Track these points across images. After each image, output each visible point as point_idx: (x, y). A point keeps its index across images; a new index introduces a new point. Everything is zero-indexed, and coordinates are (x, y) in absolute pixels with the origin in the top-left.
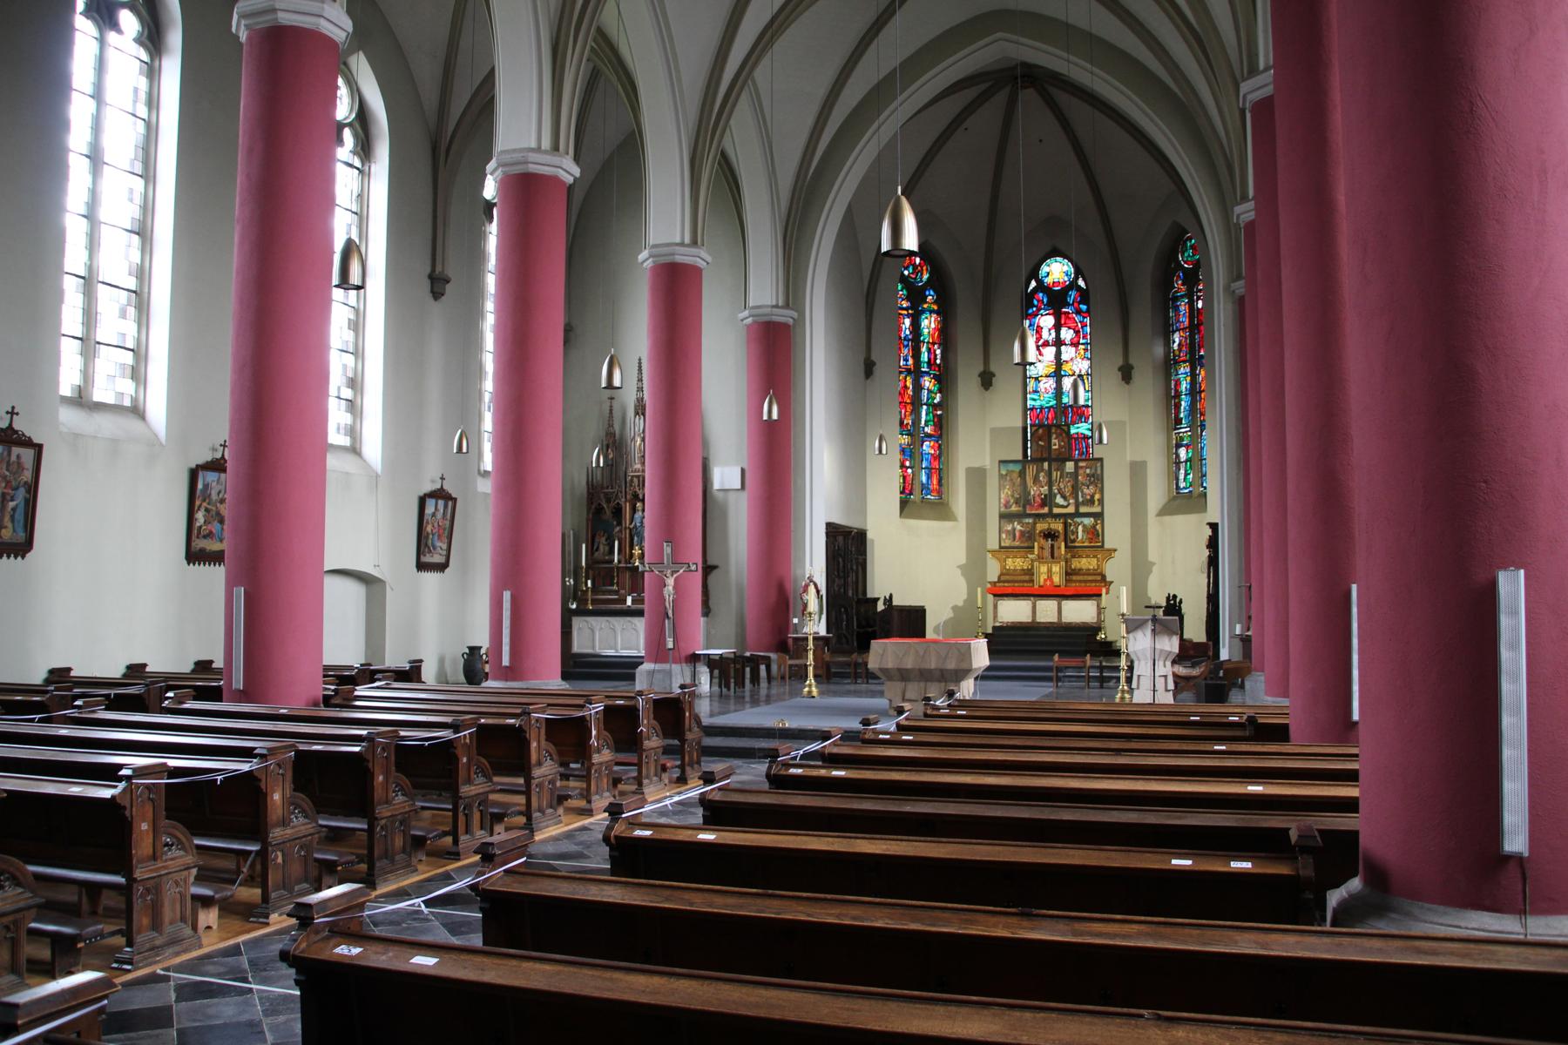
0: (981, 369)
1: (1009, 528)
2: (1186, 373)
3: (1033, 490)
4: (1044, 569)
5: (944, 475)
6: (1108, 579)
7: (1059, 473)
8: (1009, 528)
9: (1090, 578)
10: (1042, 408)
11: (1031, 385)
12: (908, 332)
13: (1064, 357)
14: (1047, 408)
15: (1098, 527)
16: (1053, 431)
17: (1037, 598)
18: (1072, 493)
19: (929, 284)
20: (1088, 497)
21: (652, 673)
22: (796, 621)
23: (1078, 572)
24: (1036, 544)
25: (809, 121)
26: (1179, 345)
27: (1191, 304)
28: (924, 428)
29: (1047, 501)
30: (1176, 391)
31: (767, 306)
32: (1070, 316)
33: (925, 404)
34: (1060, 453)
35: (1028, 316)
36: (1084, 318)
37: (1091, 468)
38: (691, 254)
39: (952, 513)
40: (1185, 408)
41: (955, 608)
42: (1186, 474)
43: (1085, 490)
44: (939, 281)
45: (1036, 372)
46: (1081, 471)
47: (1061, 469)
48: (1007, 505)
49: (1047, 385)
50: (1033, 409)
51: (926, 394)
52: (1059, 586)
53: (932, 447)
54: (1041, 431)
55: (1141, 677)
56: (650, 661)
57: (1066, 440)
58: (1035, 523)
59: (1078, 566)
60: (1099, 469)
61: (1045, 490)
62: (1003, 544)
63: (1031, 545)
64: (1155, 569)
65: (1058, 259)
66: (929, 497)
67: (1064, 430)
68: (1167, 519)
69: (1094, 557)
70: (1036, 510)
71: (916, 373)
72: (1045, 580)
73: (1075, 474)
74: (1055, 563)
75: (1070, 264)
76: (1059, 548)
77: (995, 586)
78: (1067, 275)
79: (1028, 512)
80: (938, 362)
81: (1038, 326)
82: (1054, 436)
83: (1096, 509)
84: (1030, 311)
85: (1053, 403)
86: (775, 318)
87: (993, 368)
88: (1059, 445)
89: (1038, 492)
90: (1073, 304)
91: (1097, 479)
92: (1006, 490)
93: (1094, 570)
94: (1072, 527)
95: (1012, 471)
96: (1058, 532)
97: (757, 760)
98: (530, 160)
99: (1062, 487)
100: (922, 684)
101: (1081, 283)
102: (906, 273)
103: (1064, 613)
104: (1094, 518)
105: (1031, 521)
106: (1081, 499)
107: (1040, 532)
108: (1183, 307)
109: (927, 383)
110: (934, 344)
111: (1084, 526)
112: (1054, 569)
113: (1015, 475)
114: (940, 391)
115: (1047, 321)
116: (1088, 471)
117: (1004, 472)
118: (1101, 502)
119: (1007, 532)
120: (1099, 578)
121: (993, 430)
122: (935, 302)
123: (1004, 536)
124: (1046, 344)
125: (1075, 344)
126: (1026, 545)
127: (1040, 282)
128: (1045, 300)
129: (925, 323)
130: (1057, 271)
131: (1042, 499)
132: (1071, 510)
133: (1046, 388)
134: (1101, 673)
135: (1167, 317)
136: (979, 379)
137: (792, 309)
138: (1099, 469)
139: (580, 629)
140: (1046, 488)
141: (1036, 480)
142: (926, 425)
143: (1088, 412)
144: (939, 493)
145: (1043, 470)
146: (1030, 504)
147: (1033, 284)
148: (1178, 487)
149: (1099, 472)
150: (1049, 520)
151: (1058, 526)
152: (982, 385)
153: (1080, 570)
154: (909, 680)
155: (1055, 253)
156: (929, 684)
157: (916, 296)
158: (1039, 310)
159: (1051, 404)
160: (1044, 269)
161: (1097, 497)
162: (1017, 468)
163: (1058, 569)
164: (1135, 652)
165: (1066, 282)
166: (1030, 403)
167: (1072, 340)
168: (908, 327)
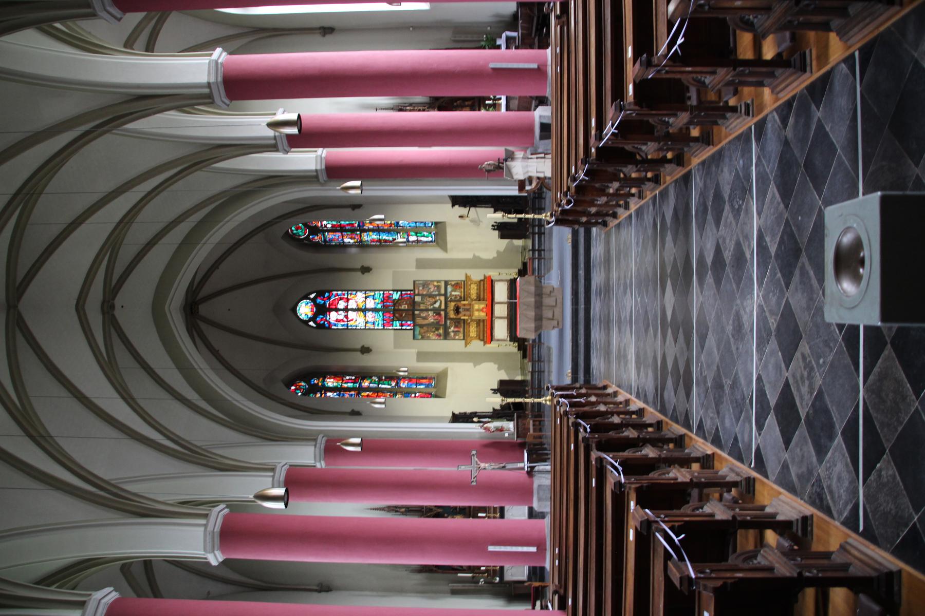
0: (359, 353)
1: (452, 334)
2: (367, 235)
3: (431, 320)
4: (476, 314)
5: (420, 376)
6: (483, 278)
8: (452, 334)
9: (482, 288)
10: (384, 320)
11: (370, 326)
12: (335, 394)
13: (354, 307)
14: (383, 317)
15: (453, 283)
18: (433, 297)
19: (308, 382)
20: (436, 288)
21: (540, 500)
22: (506, 435)
24: (462, 318)
25: (205, 422)
26: (351, 239)
27: (329, 231)
29: (437, 312)
30: (377, 241)
31: (315, 450)
33: (378, 385)
34: (410, 304)
35: (329, 328)
36: (332, 294)
38: (280, 472)
39: (443, 371)
40: (387, 236)
41: (499, 369)
42: (424, 236)
44: (306, 376)
46: (421, 292)
47: (419, 304)
48: (439, 335)
53: (404, 382)
54: (397, 315)
55: (538, 170)
56: (531, 500)
57: (403, 301)
58: (451, 319)
60: (420, 282)
61: (431, 313)
62: (462, 338)
63: (462, 321)
64: (477, 254)
65: (298, 308)
68: (449, 246)
70: (442, 318)
71: (360, 390)
72: (483, 312)
74: (473, 307)
75: (301, 302)
76: (464, 305)
78: (307, 304)
79: (443, 323)
81: (336, 321)
82: (400, 307)
83: (443, 284)
84: (327, 325)
85: (381, 313)
86: (323, 446)
87: (359, 347)
88: (405, 304)
89: (432, 317)
90: (325, 301)
91: (426, 284)
92: (431, 335)
93: (477, 286)
95: (420, 331)
96: (455, 305)
97: (591, 379)
98: (212, 529)
100: (544, 308)
101: (312, 296)
102: (300, 394)
105: (448, 322)
106: (437, 293)
107: (455, 315)
108: (330, 236)
109: (366, 384)
111: (452, 291)
113: (422, 331)
114: (371, 377)
115: (333, 316)
116: (421, 288)
117: (420, 337)
118: (438, 282)
119: (455, 335)
120: (482, 283)
121: (395, 347)
122: (318, 379)
123: (457, 337)
124: (346, 317)
125: (347, 300)
126: (462, 325)
127: (310, 319)
128: (321, 316)
129: (330, 385)
130: (305, 310)
131: (436, 315)
132: (443, 298)
133: (372, 317)
134: (536, 226)
135: (335, 246)
136: (365, 354)
137: (318, 437)
139: (512, 575)
140: (430, 312)
141: (425, 318)
143: (386, 293)
144: (431, 379)
145: (420, 314)
146: (439, 321)
147: (311, 323)
148: (431, 242)
150: (448, 310)
151: (452, 305)
153: (477, 293)
154: (542, 316)
155: (294, 310)
156: (544, 304)
157: (314, 389)
158: (326, 320)
160: (303, 317)
161: (435, 284)
162: (418, 329)
164: (524, 174)
165: (311, 305)
166: (381, 327)
167: (345, 302)
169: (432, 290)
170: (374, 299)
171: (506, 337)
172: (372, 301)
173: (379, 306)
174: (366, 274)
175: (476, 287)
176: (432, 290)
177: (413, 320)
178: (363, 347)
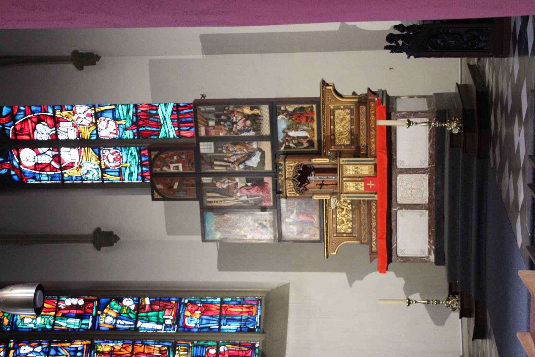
0: (89, 247)
4: (351, 186)
7: (216, 163)
9: (363, 121)
10: (141, 164)
11: (112, 178)
13: (72, 136)
14: (140, 158)
15: (291, 108)
16: (158, 170)
17: (394, 203)
18: (244, 145)
20: (248, 123)
23: (354, 138)
28: (166, 326)
32: (18, 128)
33: (136, 323)
37: (208, 119)
43: (239, 128)
45: (95, 172)
46: (213, 133)
47: (210, 160)
51: (122, 322)
52: (375, 166)
53: (192, 312)
54: (159, 186)
59: (346, 134)
67: (156, 157)
69: (332, 112)
73: (216, 140)
77: (376, 253)
80: (81, 302)
81: (35, 169)
82: (165, 169)
83: (265, 111)
87: (89, 231)
88: (177, 162)
93: (351, 114)
94: (291, 145)
96: (298, 166)
99: (235, 158)
103: (416, 164)
104: (277, 114)
106: (252, 133)
110: (57, 309)
111: (289, 128)
116: (212, 123)
118: (255, 103)
121: (170, 231)
124: (57, 158)
125: (56, 122)
131: (253, 186)
132: (266, 146)
138: (208, 109)
140: (237, 180)
145: (213, 184)
149: (213, 108)
150: (280, 180)
152: (112, 245)
153: (351, 133)
159: (135, 153)
161: (247, 111)
163: (351, 167)
169: (240, 126)
170: (115, 119)
171: (426, 254)
172: (112, 123)
173: (129, 134)
174: (86, 68)
175: (348, 117)
176: (240, 126)
177: (200, 197)
178: (98, 231)
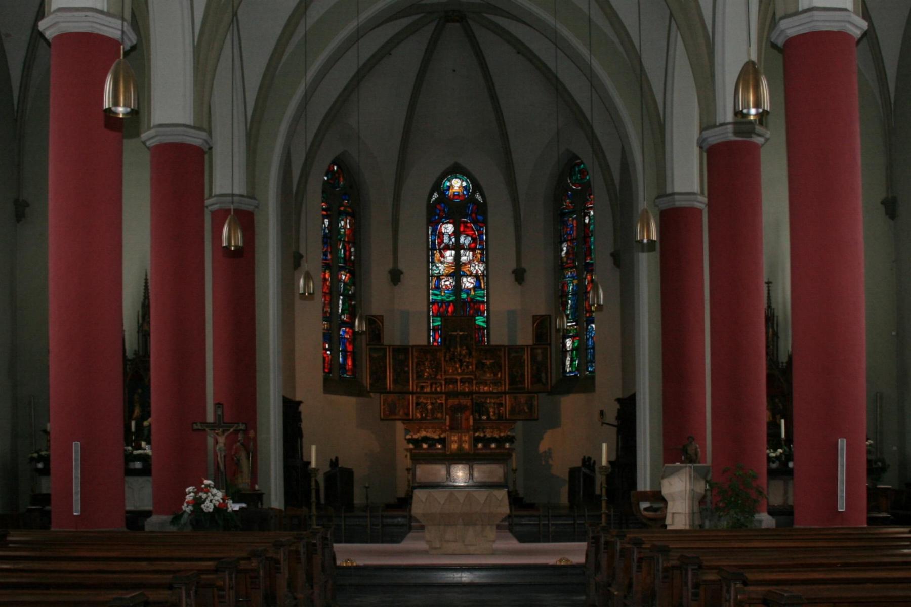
0: (391, 266)
26: (566, 253)
28: (340, 316)
42: (572, 361)
45: (438, 271)
49: (448, 283)
50: (434, 302)
66: (345, 376)
90: (471, 215)
101: (478, 197)
112: (463, 438)
125: (472, 249)
142: (343, 313)
147: (436, 196)
159: (451, 299)
163: (467, 438)
167: (469, 245)
168: (327, 225)
